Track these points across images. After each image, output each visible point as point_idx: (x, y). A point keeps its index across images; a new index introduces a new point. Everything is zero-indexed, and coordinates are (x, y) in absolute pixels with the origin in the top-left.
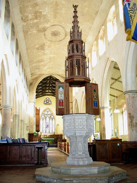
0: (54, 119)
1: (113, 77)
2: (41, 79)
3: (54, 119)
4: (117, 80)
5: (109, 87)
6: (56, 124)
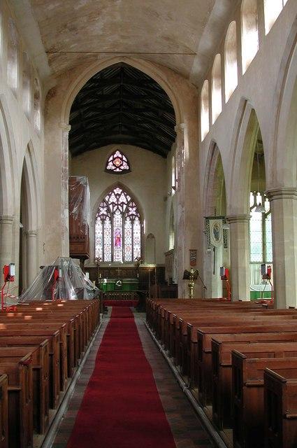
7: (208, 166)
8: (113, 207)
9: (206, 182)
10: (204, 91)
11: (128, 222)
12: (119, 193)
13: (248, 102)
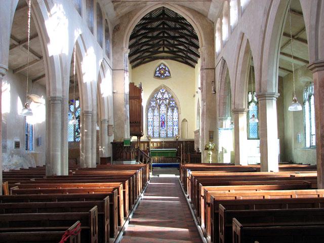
0: (175, 109)
1: (287, 32)
2: (137, 20)
3: (175, 109)
4: (296, 37)
5: (277, 51)
6: (182, 119)
7: (221, 76)
8: (160, 101)
9: (219, 86)
10: (218, 25)
11: (170, 111)
12: (164, 92)
13: (245, 35)
